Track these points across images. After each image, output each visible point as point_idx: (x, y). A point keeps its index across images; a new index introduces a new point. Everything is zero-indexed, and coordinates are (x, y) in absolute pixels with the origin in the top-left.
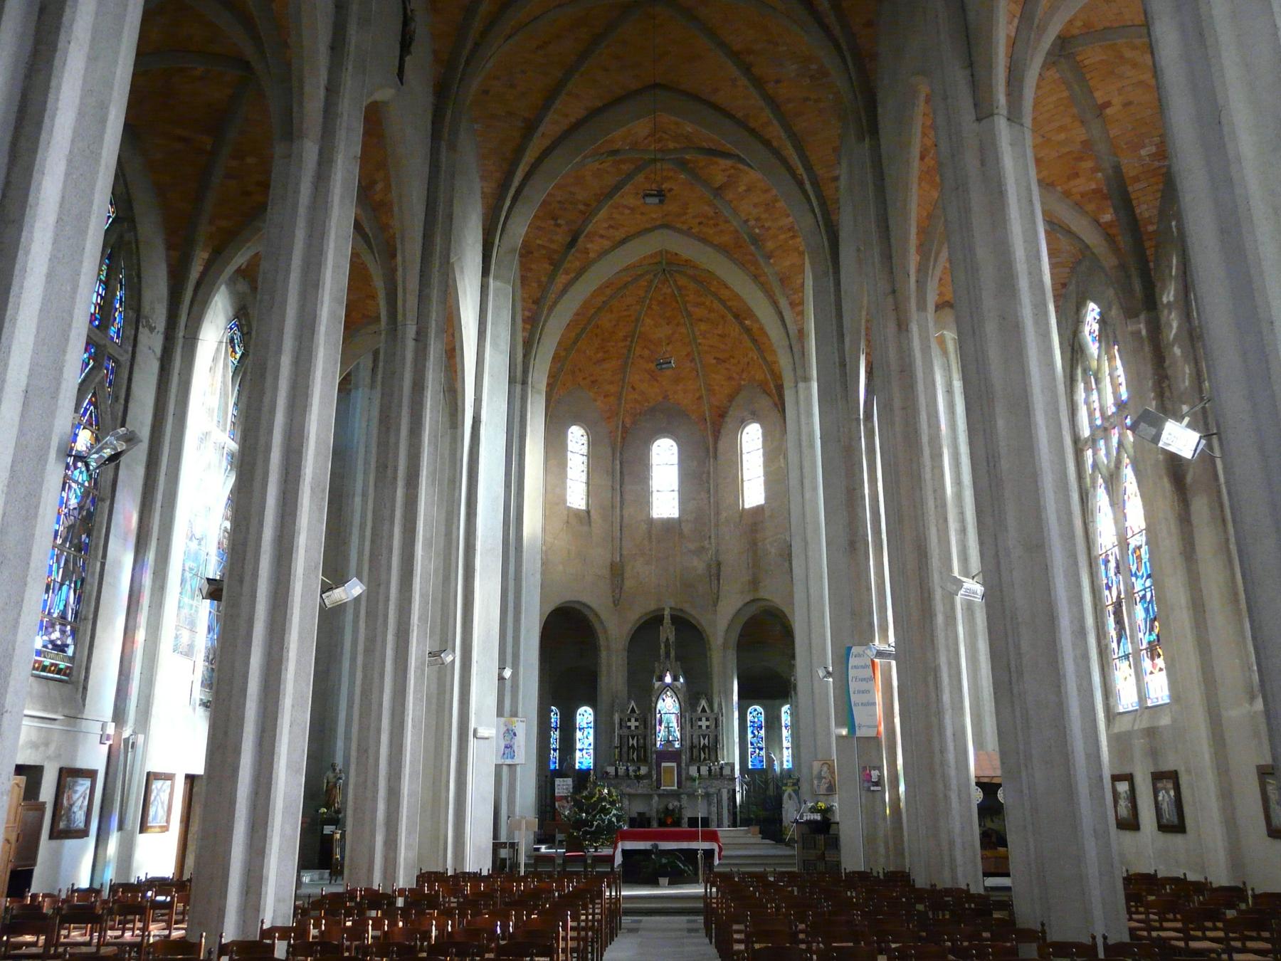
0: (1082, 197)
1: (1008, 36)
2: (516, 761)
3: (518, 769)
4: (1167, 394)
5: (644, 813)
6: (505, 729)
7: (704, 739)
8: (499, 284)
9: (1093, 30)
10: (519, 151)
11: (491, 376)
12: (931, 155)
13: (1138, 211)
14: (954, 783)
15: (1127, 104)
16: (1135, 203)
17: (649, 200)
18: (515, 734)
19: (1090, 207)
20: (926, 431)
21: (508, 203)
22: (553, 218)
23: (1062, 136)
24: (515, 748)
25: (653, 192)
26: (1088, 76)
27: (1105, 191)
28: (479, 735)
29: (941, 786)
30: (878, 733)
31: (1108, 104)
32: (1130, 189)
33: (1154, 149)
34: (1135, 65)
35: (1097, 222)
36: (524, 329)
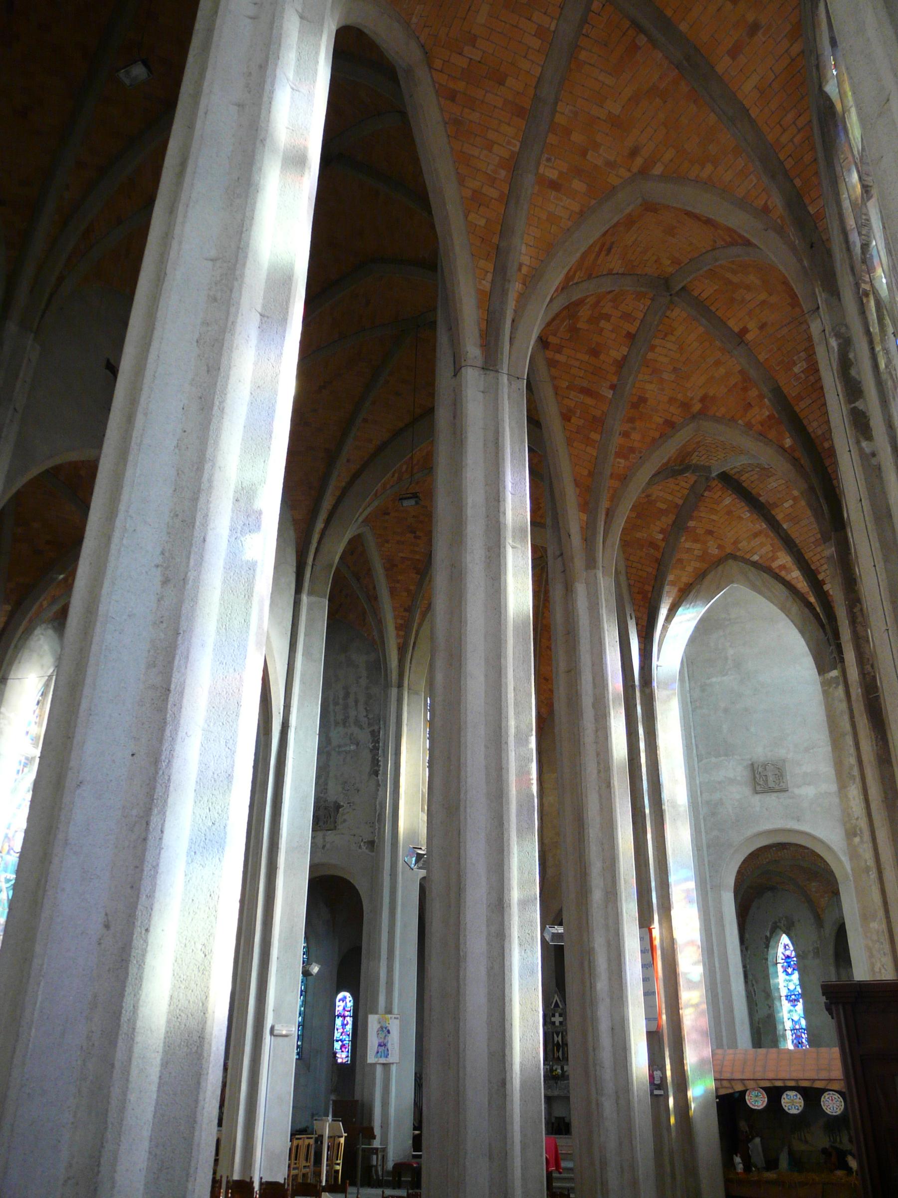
0: (762, 425)
1: (480, 292)
2: (390, 1060)
3: (394, 1068)
4: (860, 619)
5: (563, 1118)
6: (379, 1026)
7: (558, 1037)
8: (314, 599)
9: (683, 265)
10: (324, 480)
11: (303, 682)
12: (578, 415)
13: (810, 430)
14: (609, 1086)
15: (762, 327)
16: (805, 422)
17: (406, 503)
18: (389, 1032)
19: (772, 434)
20: (590, 692)
21: (319, 525)
22: (411, 532)
23: (722, 370)
24: (389, 1046)
25: (408, 495)
26: (714, 309)
27: (777, 416)
28: (276, 1032)
29: (593, 1091)
30: (659, 1026)
31: (744, 331)
32: (797, 409)
33: (804, 365)
34: (748, 288)
35: (782, 447)
36: (398, 636)
